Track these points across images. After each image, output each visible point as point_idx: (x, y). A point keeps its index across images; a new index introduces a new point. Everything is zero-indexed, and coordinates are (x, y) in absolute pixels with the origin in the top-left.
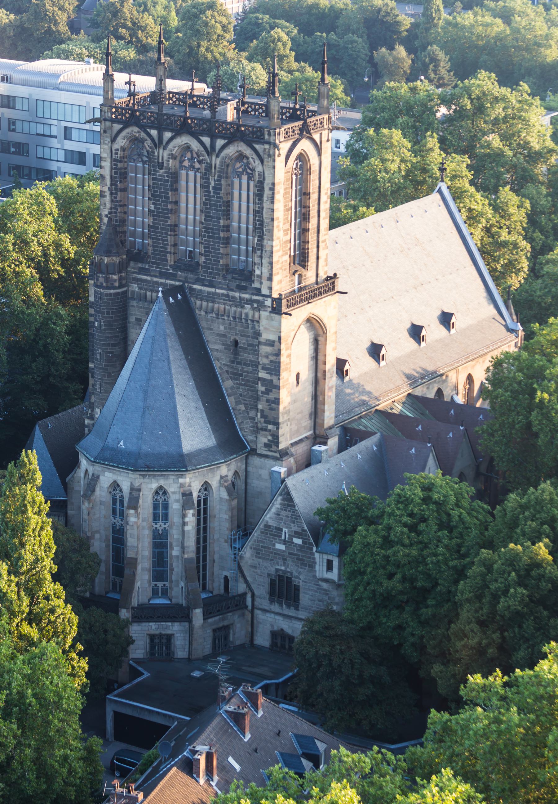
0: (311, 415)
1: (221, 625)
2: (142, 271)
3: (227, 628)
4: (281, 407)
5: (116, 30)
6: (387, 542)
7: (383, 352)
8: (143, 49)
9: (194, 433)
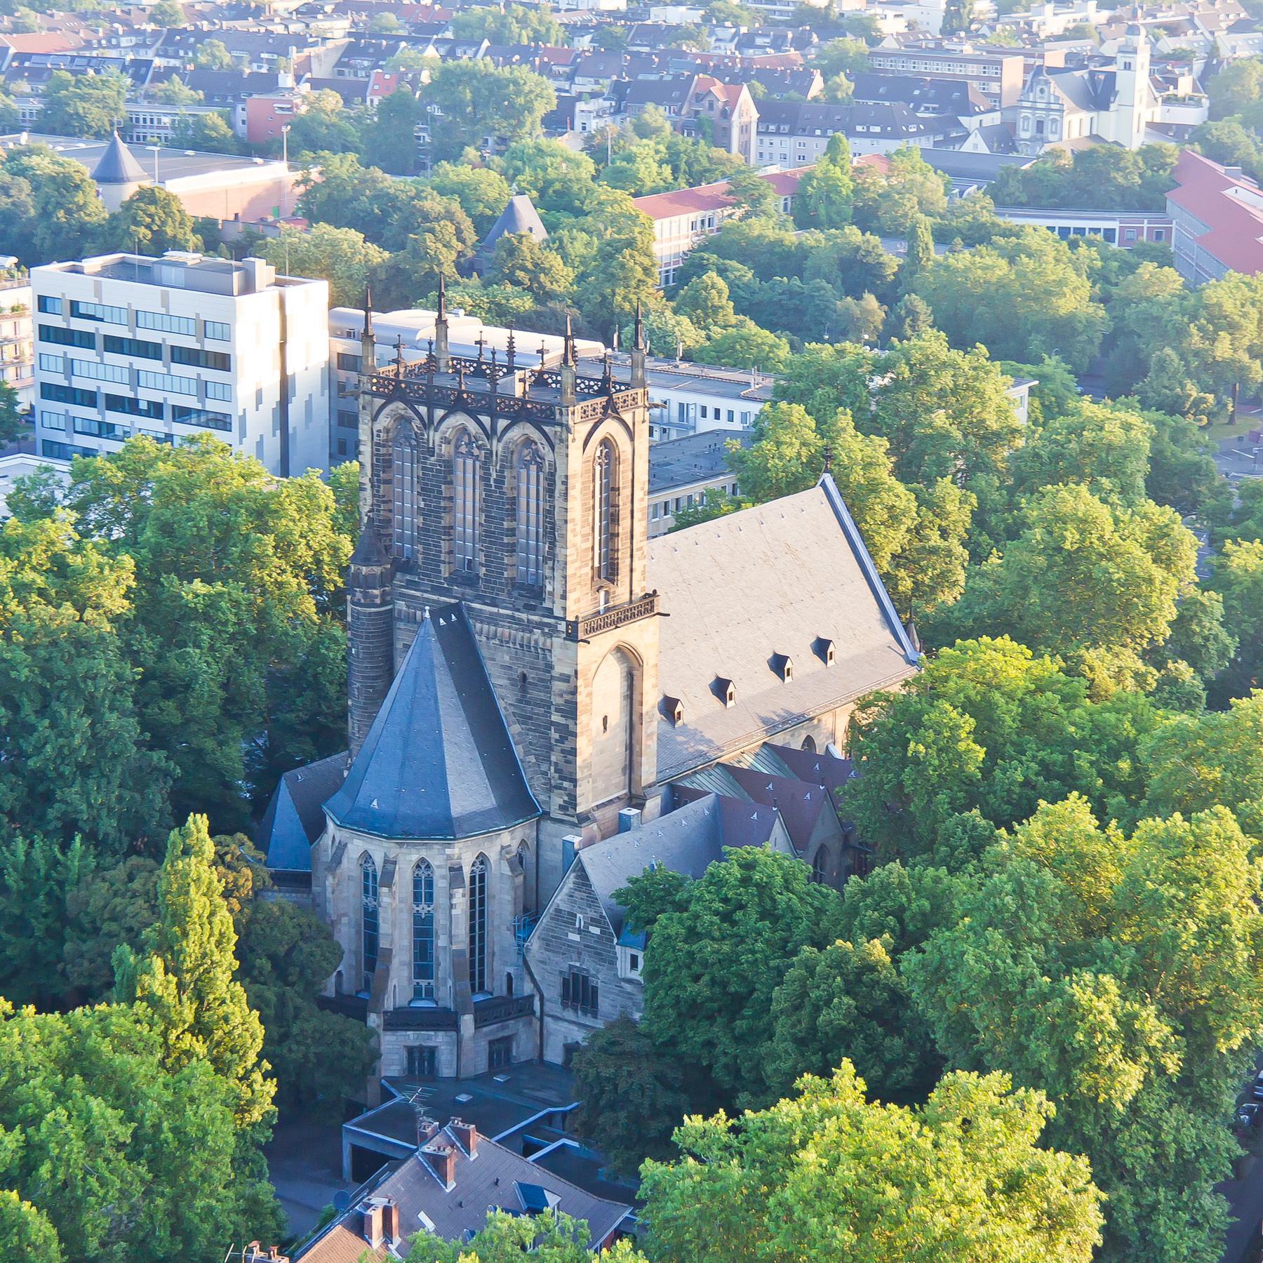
0: (624, 769)
1: (501, 1035)
2: (410, 585)
3: (508, 1040)
4: (579, 760)
5: (512, 273)
6: (693, 935)
7: (731, 689)
8: (543, 296)
9: (469, 789)
